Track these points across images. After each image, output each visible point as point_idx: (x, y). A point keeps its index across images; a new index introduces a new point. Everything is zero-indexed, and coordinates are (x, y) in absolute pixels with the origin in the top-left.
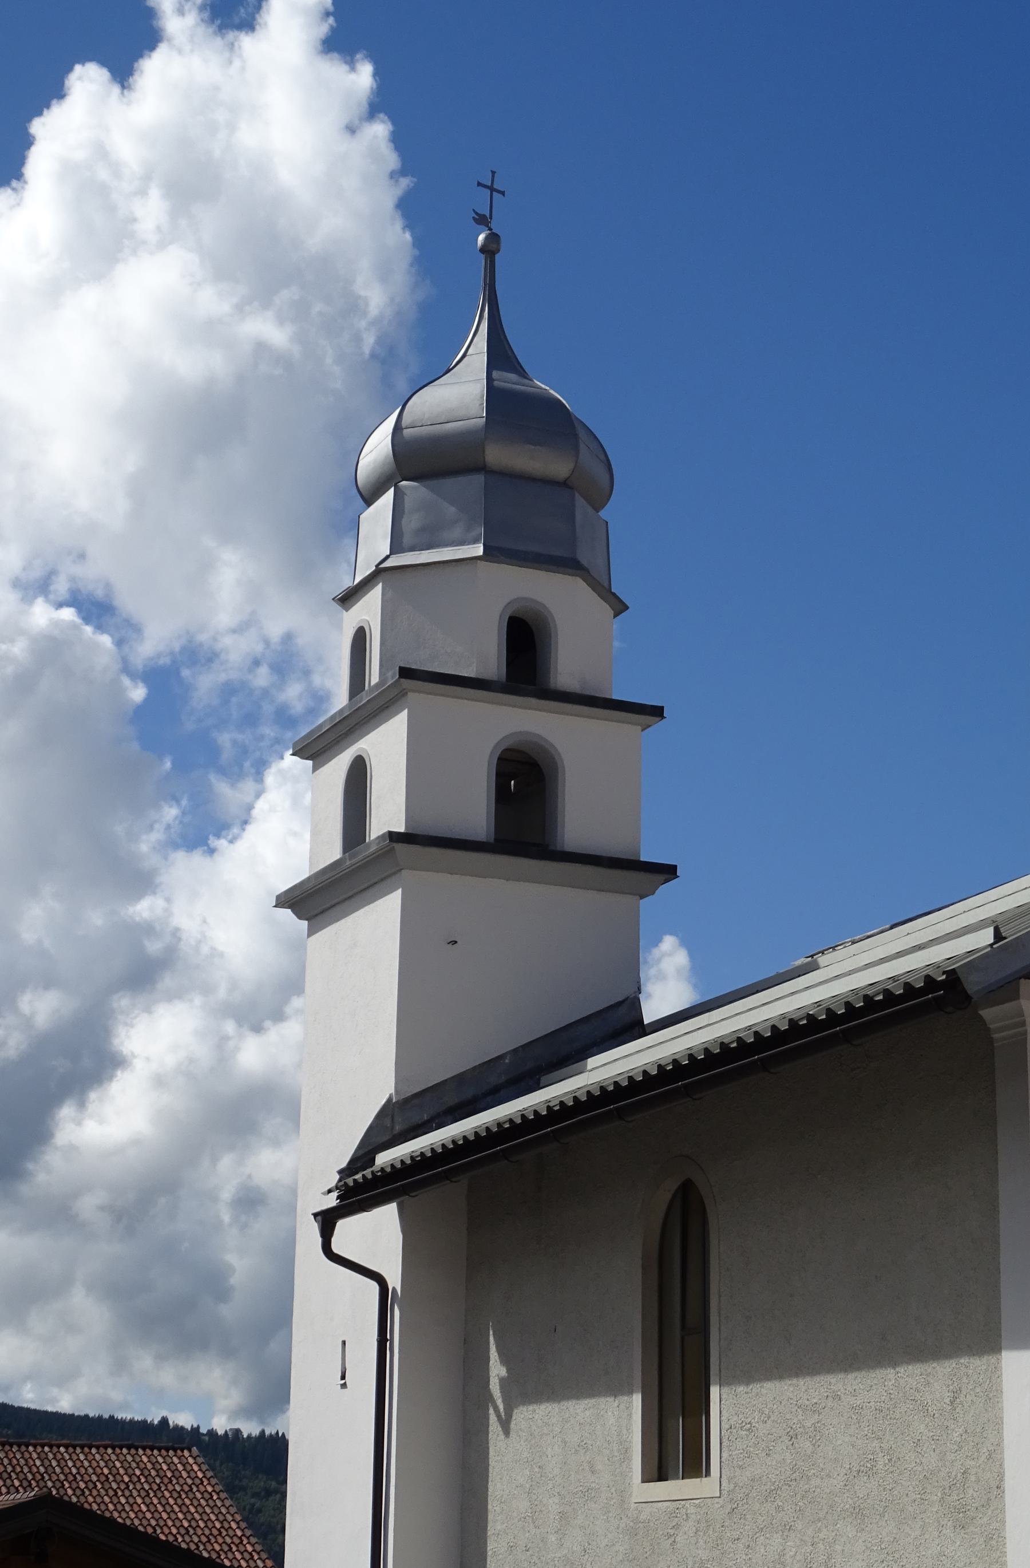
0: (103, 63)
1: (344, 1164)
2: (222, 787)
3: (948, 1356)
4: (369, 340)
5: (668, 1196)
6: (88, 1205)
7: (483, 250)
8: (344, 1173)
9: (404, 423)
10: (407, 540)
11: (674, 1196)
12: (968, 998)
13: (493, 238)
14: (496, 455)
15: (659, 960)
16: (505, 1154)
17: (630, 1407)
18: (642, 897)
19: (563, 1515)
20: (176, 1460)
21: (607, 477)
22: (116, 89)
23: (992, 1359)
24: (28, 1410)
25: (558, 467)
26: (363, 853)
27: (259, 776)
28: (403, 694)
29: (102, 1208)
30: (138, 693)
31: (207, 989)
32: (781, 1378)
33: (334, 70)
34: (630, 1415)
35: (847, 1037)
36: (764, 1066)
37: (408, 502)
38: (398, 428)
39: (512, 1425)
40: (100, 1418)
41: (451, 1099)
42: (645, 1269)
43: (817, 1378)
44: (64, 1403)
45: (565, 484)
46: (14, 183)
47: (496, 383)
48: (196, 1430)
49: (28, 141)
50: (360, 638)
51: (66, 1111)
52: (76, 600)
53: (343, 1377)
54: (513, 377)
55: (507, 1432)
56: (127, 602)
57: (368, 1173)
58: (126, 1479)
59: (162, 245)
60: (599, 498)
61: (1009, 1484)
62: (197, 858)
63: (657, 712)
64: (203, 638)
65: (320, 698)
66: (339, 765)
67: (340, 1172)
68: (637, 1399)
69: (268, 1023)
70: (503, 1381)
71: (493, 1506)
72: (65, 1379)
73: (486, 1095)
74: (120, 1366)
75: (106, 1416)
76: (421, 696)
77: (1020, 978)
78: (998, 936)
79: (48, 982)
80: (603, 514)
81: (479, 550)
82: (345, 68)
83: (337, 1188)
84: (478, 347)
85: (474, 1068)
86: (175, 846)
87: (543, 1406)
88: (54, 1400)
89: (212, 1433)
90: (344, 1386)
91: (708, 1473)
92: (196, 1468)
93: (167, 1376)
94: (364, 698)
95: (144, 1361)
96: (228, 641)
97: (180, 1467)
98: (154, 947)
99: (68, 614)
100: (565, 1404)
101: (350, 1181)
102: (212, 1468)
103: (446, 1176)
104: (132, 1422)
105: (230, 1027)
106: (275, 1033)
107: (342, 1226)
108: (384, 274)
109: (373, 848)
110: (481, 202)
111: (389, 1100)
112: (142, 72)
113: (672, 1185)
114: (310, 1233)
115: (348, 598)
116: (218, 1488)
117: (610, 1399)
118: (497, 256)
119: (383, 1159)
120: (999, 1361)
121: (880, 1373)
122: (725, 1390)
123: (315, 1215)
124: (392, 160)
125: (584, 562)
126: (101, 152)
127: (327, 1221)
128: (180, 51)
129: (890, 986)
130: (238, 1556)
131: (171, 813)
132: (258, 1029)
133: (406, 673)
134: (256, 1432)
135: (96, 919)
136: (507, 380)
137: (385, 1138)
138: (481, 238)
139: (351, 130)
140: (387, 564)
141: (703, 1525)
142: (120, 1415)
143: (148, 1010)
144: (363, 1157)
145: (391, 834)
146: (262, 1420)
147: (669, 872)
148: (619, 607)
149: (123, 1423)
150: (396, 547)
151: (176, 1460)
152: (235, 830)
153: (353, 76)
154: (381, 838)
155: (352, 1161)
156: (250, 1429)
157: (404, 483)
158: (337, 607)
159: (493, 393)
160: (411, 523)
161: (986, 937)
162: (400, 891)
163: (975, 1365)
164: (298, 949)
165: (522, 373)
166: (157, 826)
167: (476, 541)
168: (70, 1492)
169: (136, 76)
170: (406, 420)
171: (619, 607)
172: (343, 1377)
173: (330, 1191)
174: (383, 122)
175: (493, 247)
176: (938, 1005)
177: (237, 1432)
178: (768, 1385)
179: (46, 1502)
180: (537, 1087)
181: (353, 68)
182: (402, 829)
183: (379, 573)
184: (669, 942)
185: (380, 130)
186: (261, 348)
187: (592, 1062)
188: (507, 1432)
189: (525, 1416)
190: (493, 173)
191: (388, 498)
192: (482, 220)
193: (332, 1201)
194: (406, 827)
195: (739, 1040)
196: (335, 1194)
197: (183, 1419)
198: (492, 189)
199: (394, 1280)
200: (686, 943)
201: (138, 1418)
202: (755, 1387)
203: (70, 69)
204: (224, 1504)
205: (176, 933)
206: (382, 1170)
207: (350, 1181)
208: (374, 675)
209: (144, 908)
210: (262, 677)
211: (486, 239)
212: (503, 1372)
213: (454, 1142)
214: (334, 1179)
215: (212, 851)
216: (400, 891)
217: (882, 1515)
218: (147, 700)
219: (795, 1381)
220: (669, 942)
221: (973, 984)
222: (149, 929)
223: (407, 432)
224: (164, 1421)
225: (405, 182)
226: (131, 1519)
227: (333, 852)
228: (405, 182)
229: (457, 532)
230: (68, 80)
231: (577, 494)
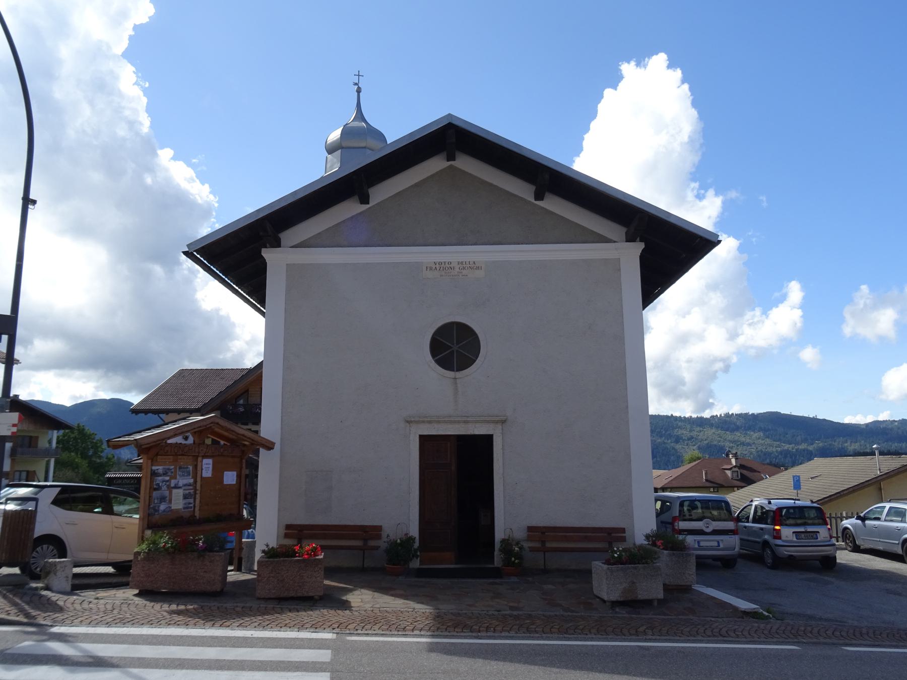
40: (656, 415)
104: (664, 416)
118: (361, 94)
185: (686, 87)
190: (359, 71)
201: (665, 414)
224: (672, 415)
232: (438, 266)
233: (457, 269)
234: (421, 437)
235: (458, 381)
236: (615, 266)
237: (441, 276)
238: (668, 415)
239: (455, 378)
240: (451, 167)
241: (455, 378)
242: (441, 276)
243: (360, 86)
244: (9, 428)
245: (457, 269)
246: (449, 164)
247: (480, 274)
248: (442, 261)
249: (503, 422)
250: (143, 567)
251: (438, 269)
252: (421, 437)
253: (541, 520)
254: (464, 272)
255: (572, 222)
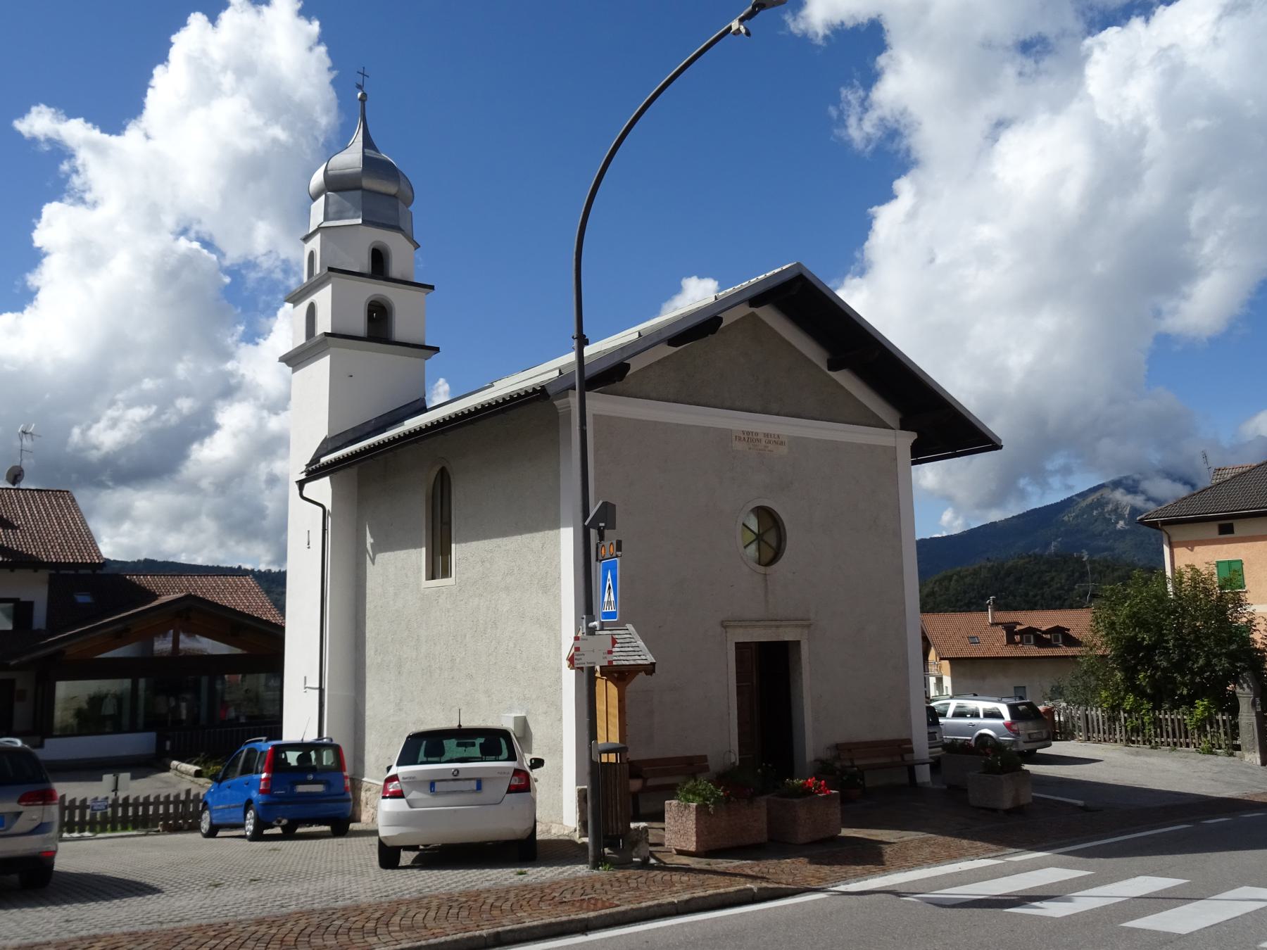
0: (204, 12)
1: (308, 462)
2: (263, 320)
3: (541, 531)
4: (321, 140)
5: (436, 473)
6: (205, 484)
7: (360, 99)
8: (308, 466)
9: (328, 169)
10: (331, 216)
11: (438, 473)
12: (549, 396)
13: (364, 95)
14: (367, 183)
15: (437, 388)
16: (371, 457)
17: (421, 553)
18: (426, 359)
19: (395, 594)
20: (243, 580)
21: (411, 194)
22: (210, 25)
23: (557, 531)
24: (183, 564)
25: (391, 189)
26: (313, 341)
27: (275, 315)
28: (329, 278)
29: (210, 483)
30: (227, 280)
31: (256, 398)
32: (478, 540)
33: (303, 23)
34: (421, 556)
35: (503, 411)
36: (472, 422)
37: (331, 200)
38: (326, 171)
39: (376, 560)
40: (213, 566)
41: (351, 437)
42: (427, 501)
43: (492, 540)
44: (200, 560)
45: (394, 196)
46: (166, 63)
47: (366, 154)
48: (253, 570)
49: (171, 44)
50: (312, 255)
51: (195, 446)
52: (198, 239)
53: (308, 544)
54: (373, 152)
55: (373, 563)
56: (220, 242)
57: (317, 466)
58: (223, 588)
59: (233, 95)
60: (409, 201)
61: (562, 577)
62: (251, 346)
63: (432, 287)
64: (251, 258)
65: (301, 280)
66: (304, 306)
67: (306, 465)
68: (424, 549)
69: (280, 412)
70: (372, 544)
71: (368, 591)
72: (198, 551)
73: (364, 435)
74: (222, 545)
75: (216, 565)
76: (337, 278)
77: (568, 389)
78: (561, 373)
79: (188, 395)
80: (410, 208)
81: (360, 221)
82: (307, 22)
83: (305, 471)
84: (358, 139)
85: (360, 425)
86: (241, 341)
87: (388, 553)
88: (195, 560)
89: (259, 571)
90: (309, 548)
91: (451, 576)
92: (251, 583)
93: (241, 549)
94: (314, 279)
95: (231, 543)
96: (261, 259)
97: (245, 583)
98: (233, 381)
99: (196, 245)
100: (396, 552)
101: (310, 469)
102: (260, 585)
103: (349, 466)
104: (227, 568)
105: (265, 413)
106: (283, 415)
107: (307, 486)
108: (327, 111)
109: (318, 339)
110: (359, 79)
111: (326, 438)
112: (221, 20)
113: (437, 468)
114: (294, 489)
115: (307, 239)
116: (261, 590)
117: (413, 550)
118: (366, 103)
119: (324, 460)
120: (559, 532)
121: (516, 537)
122: (458, 545)
123: (297, 482)
124: (328, 62)
125: (402, 227)
126: (204, 52)
127: (301, 484)
128: (236, 10)
129: (519, 392)
130: (269, 616)
131: (241, 328)
132: (277, 414)
133: (330, 269)
134: (277, 570)
135: (209, 370)
136: (371, 153)
137: (324, 452)
138: (359, 94)
139: (311, 49)
140: (322, 226)
141: (449, 595)
142: (221, 565)
143: (230, 405)
144: (315, 459)
145: (325, 333)
146: (280, 566)
147: (437, 350)
148: (417, 246)
149: (223, 568)
150: (326, 219)
151: (243, 580)
152: (266, 336)
153: (310, 26)
154: (321, 334)
155: (311, 461)
156: (275, 569)
157: (329, 193)
158: (302, 242)
159: (366, 160)
160: (332, 209)
161: (556, 373)
162: (329, 356)
163: (551, 533)
164: (289, 382)
165: (377, 151)
166: (236, 334)
167: (358, 217)
168: (199, 593)
169: (219, 21)
170: (329, 167)
171: (417, 246)
172: (308, 544)
173: (302, 473)
174: (323, 46)
175: (364, 98)
176: (537, 399)
177: (270, 570)
178: (473, 543)
179: (189, 597)
180: (385, 431)
181: (310, 21)
182: (329, 331)
183: (319, 229)
184: (442, 381)
185: (322, 49)
186: (275, 141)
187: (406, 422)
188: (373, 563)
189: (382, 557)
191: (323, 198)
192: (360, 87)
193: (303, 476)
194: (332, 330)
195: (462, 412)
196: (304, 474)
197: (249, 567)
198: (363, 74)
199: (329, 507)
200: (448, 381)
201: (229, 566)
202: (469, 544)
203: (189, 15)
204: (263, 596)
205: (243, 376)
206: (323, 464)
207: (310, 469)
208: (317, 270)
209: (230, 366)
210: (278, 275)
211: (361, 95)
212: (372, 541)
213: (351, 453)
214: (304, 468)
215: (257, 344)
216: (329, 356)
217: (516, 590)
218: (231, 283)
219: (484, 541)
220: (442, 381)
221: (550, 391)
222: (232, 374)
223: (329, 172)
224: (240, 567)
225: (335, 72)
226: (225, 603)
227: (302, 340)
228: (335, 72)
229: (351, 213)
230: (877, 89)
231: (400, 202)
232: (746, 436)
233: (763, 443)
234: (737, 644)
235: (768, 577)
236: (892, 452)
237: (750, 449)
238: (234, 566)
239: (765, 574)
240: (753, 314)
241: (765, 574)
242: (750, 449)
243: (365, 92)
244: (606, 655)
245: (763, 443)
246: (751, 311)
247: (784, 450)
248: (750, 430)
249: (809, 626)
250: (706, 823)
251: (746, 440)
252: (737, 644)
253: (840, 738)
254: (771, 447)
255: (859, 401)
